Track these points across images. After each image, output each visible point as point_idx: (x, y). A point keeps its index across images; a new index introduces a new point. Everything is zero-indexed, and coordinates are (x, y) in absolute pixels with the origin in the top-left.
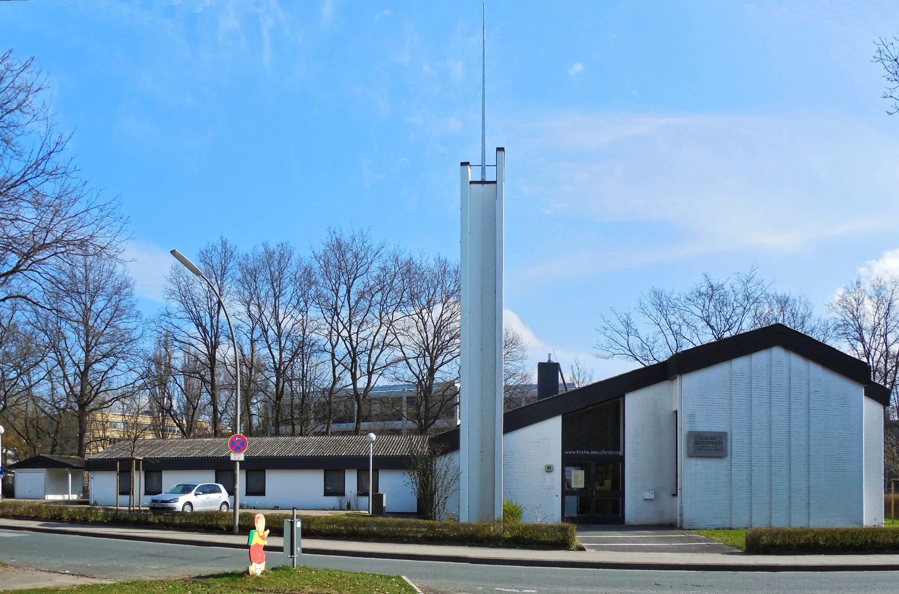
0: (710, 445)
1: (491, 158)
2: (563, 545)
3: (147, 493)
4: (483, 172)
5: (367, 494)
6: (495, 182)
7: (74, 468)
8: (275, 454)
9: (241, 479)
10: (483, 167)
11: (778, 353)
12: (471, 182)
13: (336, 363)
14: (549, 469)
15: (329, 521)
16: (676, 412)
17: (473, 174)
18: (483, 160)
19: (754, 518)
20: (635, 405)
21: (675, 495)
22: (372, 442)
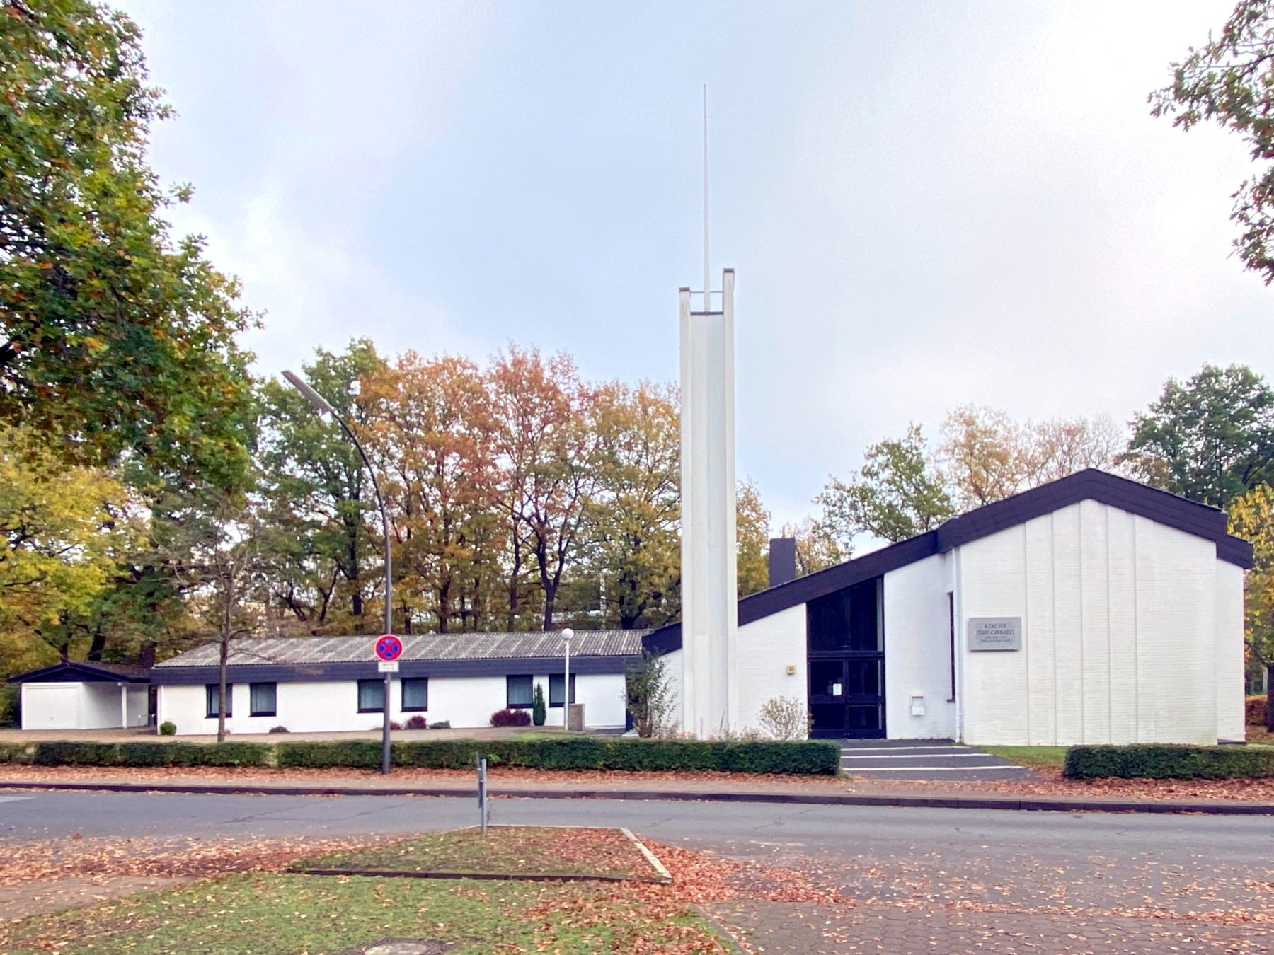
0: (998, 636)
1: (717, 282)
2: (828, 770)
3: (404, 710)
4: (707, 301)
5: (561, 705)
6: (722, 313)
7: (132, 681)
8: (441, 656)
9: (395, 689)
10: (706, 293)
11: (1089, 507)
12: (693, 314)
13: (520, 542)
14: (791, 672)
15: (127, 748)
16: (951, 595)
17: (697, 304)
18: (707, 282)
19: (1087, 732)
20: (896, 585)
21: (953, 700)
22: (568, 643)
